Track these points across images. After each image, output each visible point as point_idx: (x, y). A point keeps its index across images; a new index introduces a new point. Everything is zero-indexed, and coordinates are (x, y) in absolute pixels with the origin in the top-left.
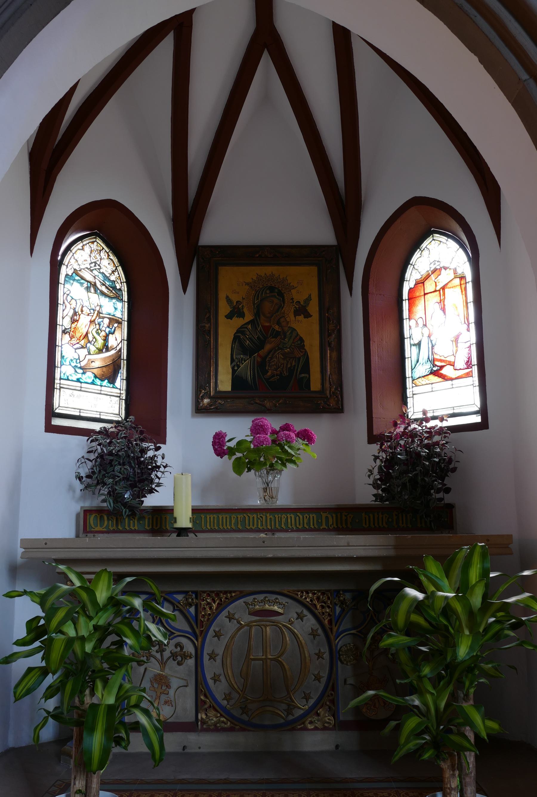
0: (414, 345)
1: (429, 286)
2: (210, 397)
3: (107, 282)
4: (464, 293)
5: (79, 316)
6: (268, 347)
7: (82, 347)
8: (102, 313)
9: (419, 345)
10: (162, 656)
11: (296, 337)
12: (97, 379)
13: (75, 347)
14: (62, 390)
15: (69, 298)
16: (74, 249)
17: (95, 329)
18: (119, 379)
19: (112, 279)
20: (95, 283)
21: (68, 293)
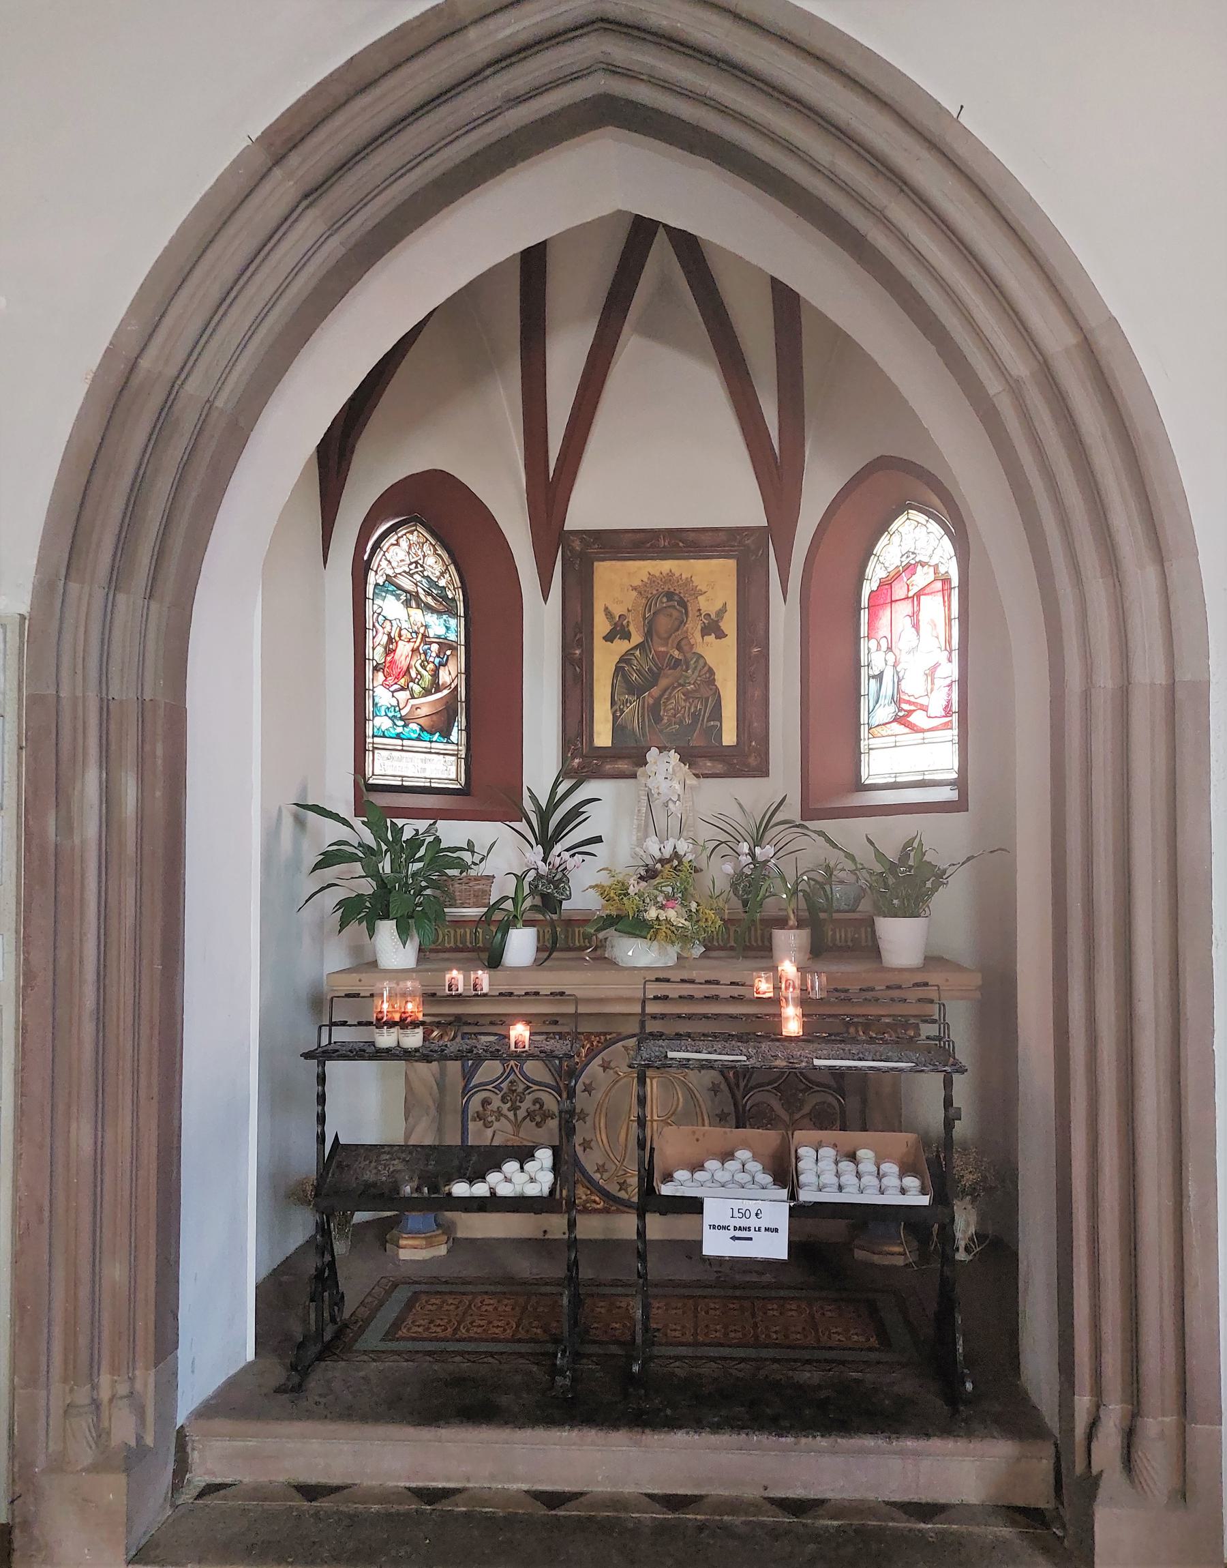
0: (874, 677)
1: (899, 591)
2: (582, 756)
3: (433, 590)
4: (947, 604)
5: (397, 643)
6: (663, 682)
7: (402, 689)
8: (429, 637)
9: (879, 677)
10: (515, 1115)
11: (704, 667)
12: (425, 733)
13: (392, 689)
14: (376, 751)
15: (381, 619)
16: (385, 545)
17: (420, 661)
18: (455, 729)
19: (440, 585)
20: (417, 592)
21: (379, 611)
